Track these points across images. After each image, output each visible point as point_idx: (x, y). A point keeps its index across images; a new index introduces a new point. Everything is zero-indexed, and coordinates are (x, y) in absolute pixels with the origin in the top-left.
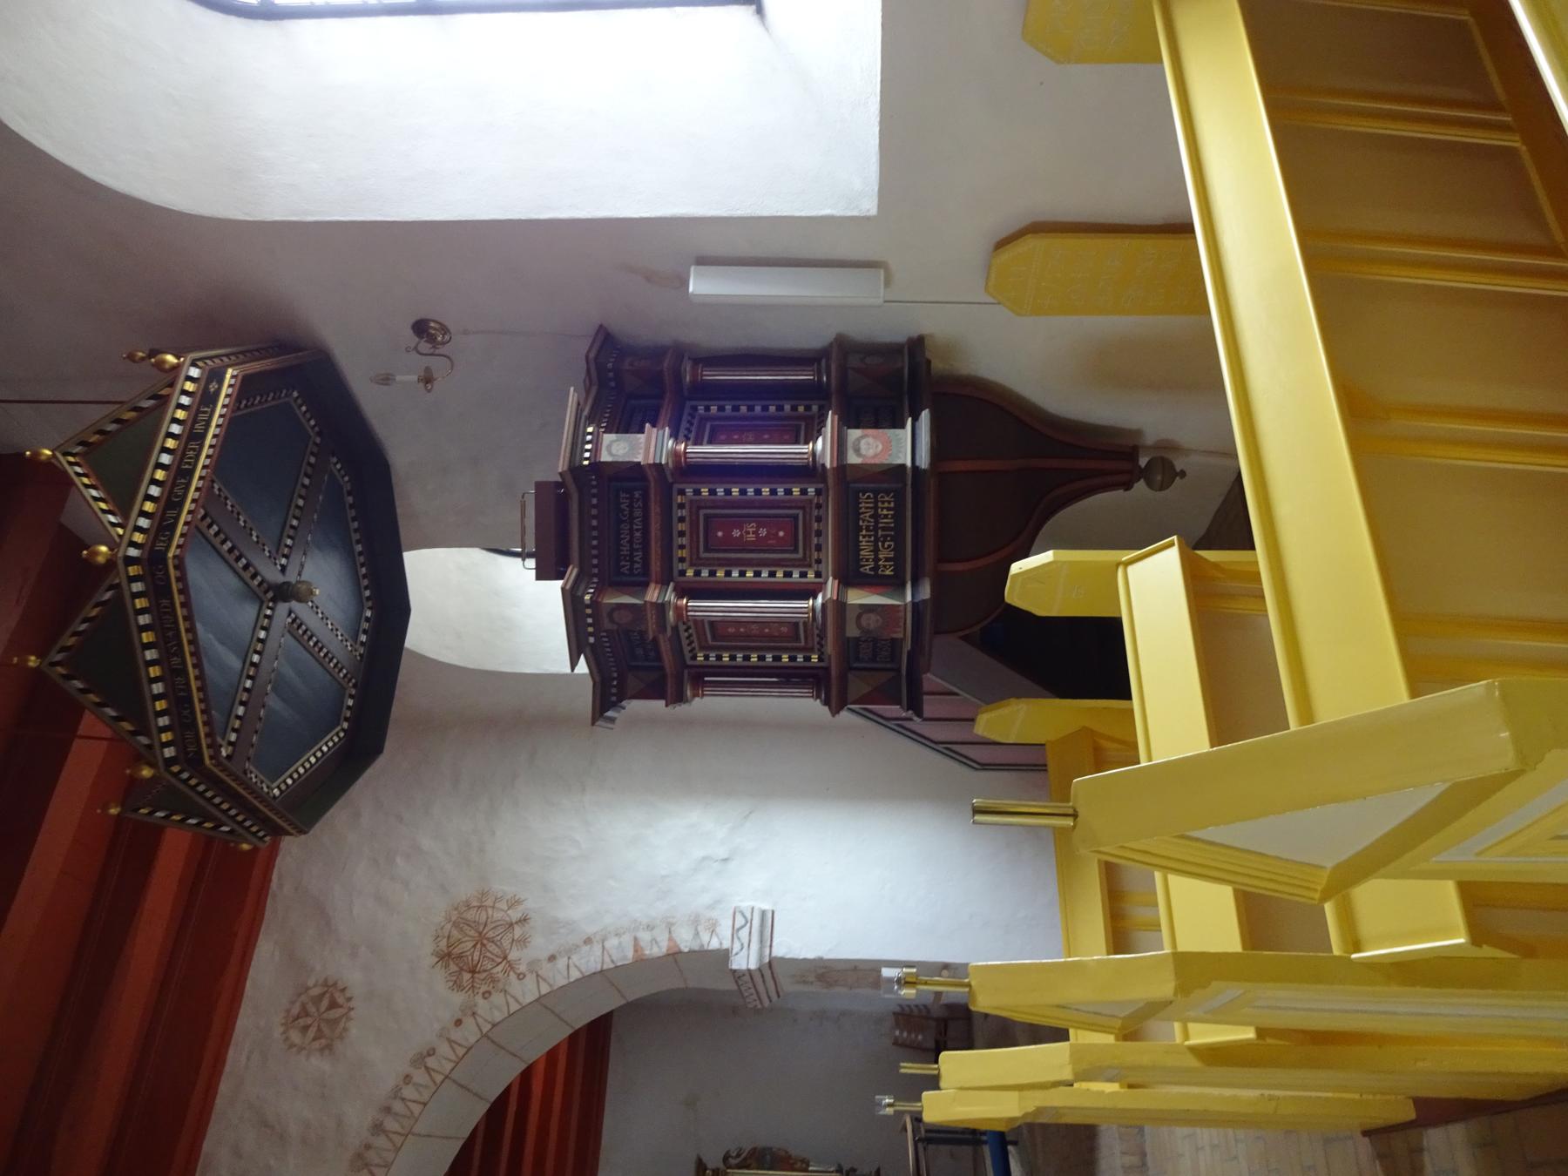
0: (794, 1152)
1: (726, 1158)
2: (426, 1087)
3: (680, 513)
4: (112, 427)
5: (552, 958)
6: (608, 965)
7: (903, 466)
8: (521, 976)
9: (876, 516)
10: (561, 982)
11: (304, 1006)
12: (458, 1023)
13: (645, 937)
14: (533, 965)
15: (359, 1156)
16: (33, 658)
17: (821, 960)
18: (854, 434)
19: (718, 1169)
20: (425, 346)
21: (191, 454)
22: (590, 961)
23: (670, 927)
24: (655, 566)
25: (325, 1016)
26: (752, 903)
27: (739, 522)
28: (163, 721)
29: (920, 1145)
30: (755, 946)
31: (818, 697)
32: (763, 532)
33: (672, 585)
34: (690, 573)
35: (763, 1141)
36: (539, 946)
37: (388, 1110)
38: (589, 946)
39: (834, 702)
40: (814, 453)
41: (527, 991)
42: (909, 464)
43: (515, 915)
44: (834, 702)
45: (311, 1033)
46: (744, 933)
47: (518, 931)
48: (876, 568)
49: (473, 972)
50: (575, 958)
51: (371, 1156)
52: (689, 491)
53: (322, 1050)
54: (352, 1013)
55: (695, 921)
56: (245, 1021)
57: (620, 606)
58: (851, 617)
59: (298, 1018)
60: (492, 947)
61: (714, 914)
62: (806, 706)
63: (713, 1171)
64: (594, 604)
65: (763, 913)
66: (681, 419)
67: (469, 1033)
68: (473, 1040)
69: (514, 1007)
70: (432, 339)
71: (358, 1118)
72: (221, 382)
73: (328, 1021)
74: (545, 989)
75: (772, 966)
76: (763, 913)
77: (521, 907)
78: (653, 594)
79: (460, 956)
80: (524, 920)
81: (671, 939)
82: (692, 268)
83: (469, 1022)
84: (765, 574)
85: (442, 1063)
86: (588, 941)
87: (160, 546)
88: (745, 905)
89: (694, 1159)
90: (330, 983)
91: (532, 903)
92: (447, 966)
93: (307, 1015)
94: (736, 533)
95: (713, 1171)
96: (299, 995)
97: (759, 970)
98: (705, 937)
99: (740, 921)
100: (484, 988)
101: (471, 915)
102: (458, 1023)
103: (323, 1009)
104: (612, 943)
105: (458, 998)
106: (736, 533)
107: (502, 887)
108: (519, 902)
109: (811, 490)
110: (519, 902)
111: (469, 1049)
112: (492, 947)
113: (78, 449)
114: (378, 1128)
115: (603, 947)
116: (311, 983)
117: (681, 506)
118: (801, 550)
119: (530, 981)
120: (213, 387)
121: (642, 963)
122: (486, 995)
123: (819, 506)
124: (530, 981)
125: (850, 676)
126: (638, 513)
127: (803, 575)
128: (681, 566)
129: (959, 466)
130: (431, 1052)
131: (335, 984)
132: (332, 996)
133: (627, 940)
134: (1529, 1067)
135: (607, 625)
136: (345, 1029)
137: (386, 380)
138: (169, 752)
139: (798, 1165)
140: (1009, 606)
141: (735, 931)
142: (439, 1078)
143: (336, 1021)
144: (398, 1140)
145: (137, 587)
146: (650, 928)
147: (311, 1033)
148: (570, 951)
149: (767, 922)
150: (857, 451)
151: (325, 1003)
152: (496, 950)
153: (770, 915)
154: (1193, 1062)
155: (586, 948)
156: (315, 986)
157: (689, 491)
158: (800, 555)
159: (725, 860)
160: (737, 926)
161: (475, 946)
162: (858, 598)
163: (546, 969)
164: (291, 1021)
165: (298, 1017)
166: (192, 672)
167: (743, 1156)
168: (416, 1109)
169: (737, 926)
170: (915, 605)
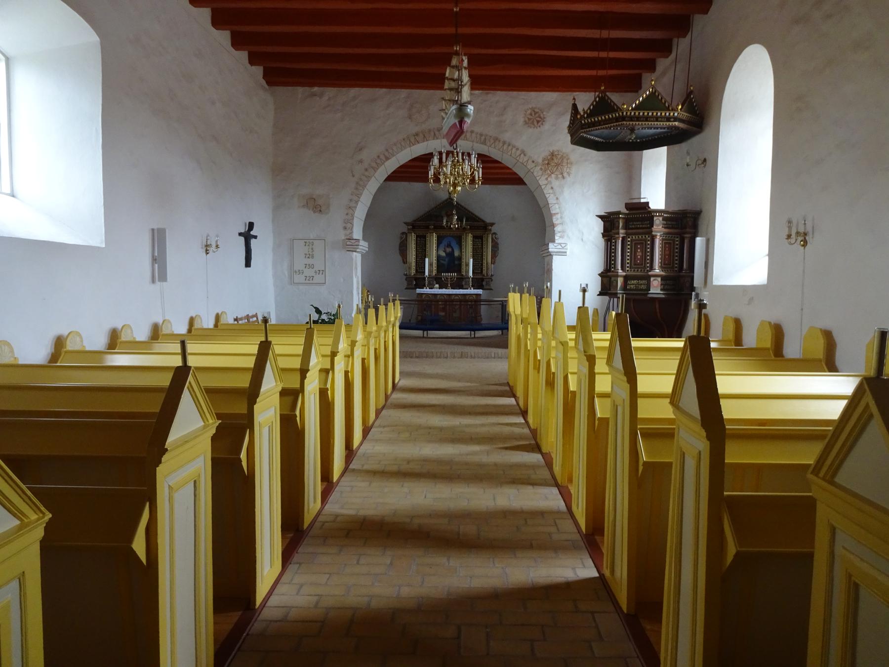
1: (495, 233)
2: (515, 155)
3: (644, 236)
4: (660, 98)
5: (552, 188)
6: (550, 206)
7: (650, 290)
8: (547, 179)
9: (641, 284)
10: (545, 192)
11: (537, 113)
12: (533, 162)
13: (559, 216)
14: (550, 182)
15: (497, 139)
16: (602, 88)
17: (552, 270)
18: (659, 279)
19: (491, 231)
20: (700, 162)
21: (652, 119)
22: (551, 200)
23: (562, 224)
24: (630, 231)
25: (535, 120)
26: (569, 248)
27: (642, 251)
28: (589, 120)
29: (501, 303)
30: (556, 250)
31: (604, 270)
32: (639, 257)
33: (625, 235)
34: (629, 239)
36: (555, 183)
37: (509, 145)
39: (602, 274)
40: (655, 269)
41: (542, 182)
42: (650, 292)
43: (565, 174)
44: (602, 274)
45: (530, 117)
46: (559, 247)
47: (560, 176)
48: (629, 284)
49: (548, 164)
50: (552, 195)
51: (497, 143)
52: (649, 239)
53: (525, 121)
54: (535, 128)
55: (563, 231)
56: (533, 94)
57: (619, 223)
58: (616, 278)
59: (534, 112)
60: (555, 168)
61: (565, 237)
62: (601, 269)
64: (619, 218)
65: (566, 252)
67: (530, 165)
68: (529, 167)
69: (538, 178)
70: (703, 163)
71: (507, 136)
72: (674, 121)
73: (533, 122)
74: (543, 187)
75: (550, 255)
76: (566, 252)
77: (567, 176)
78: (622, 231)
79: (553, 159)
80: (563, 177)
81: (558, 224)
82: (705, 238)
83: (534, 165)
84: (628, 258)
85: (523, 159)
86: (557, 199)
87: (627, 119)
88: (568, 247)
89: (494, 222)
90: (545, 120)
91: (569, 179)
92: (550, 155)
93: (535, 114)
94: (639, 250)
96: (541, 110)
97: (549, 252)
98: (559, 235)
99: (563, 245)
100: (543, 168)
101: (565, 160)
102: (533, 162)
103: (537, 119)
104: (557, 206)
105: (540, 160)
106: (639, 250)
107: (574, 169)
108: (569, 175)
109: (676, 269)
110: (569, 175)
111: (526, 166)
112: (555, 168)
113: (654, 91)
114: (504, 143)
115: (555, 204)
116: (544, 113)
117: (645, 237)
118: (664, 266)
119: (546, 182)
120: (672, 120)
121: (551, 216)
122: (541, 169)
123: (673, 271)
124: (546, 182)
125: (608, 278)
126: (644, 226)
127: (628, 267)
128: (631, 237)
129: (657, 306)
130: (525, 155)
131: (544, 121)
132: (540, 121)
133: (557, 211)
134: (518, 389)
135: (615, 220)
136: (531, 127)
137: (688, 153)
138: (583, 122)
139: (493, 260)
141: (560, 244)
142: (518, 159)
143: (533, 123)
144: (501, 150)
145: (617, 115)
146: (561, 218)
147: (530, 117)
148: (554, 193)
149: (564, 254)
150: (655, 280)
151: (538, 119)
152: (554, 170)
153: (565, 254)
154: (518, 333)
155: (555, 198)
156: (544, 115)
157: (649, 239)
158: (633, 266)
159: (582, 240)
160: (562, 245)
161: (555, 163)
162: (620, 281)
163: (549, 186)
164: (533, 109)
165: (534, 111)
166: (600, 127)
168: (509, 154)
169: (562, 245)
170: (617, 293)
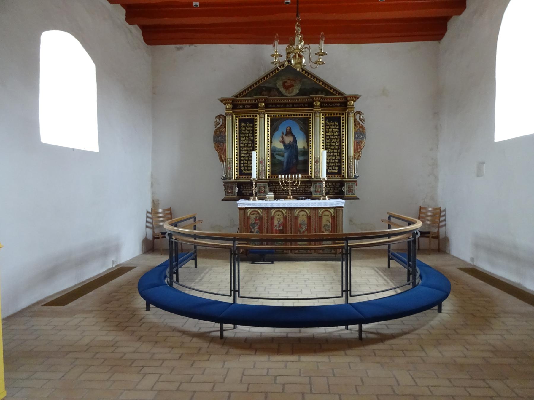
0: (363, 151)
1: (359, 113)
19: (353, 108)
35: (368, 132)
38: (332, 376)
63: (353, 105)
66: (360, 313)
95: (353, 105)
140: (136, 24)
167: (360, 122)
